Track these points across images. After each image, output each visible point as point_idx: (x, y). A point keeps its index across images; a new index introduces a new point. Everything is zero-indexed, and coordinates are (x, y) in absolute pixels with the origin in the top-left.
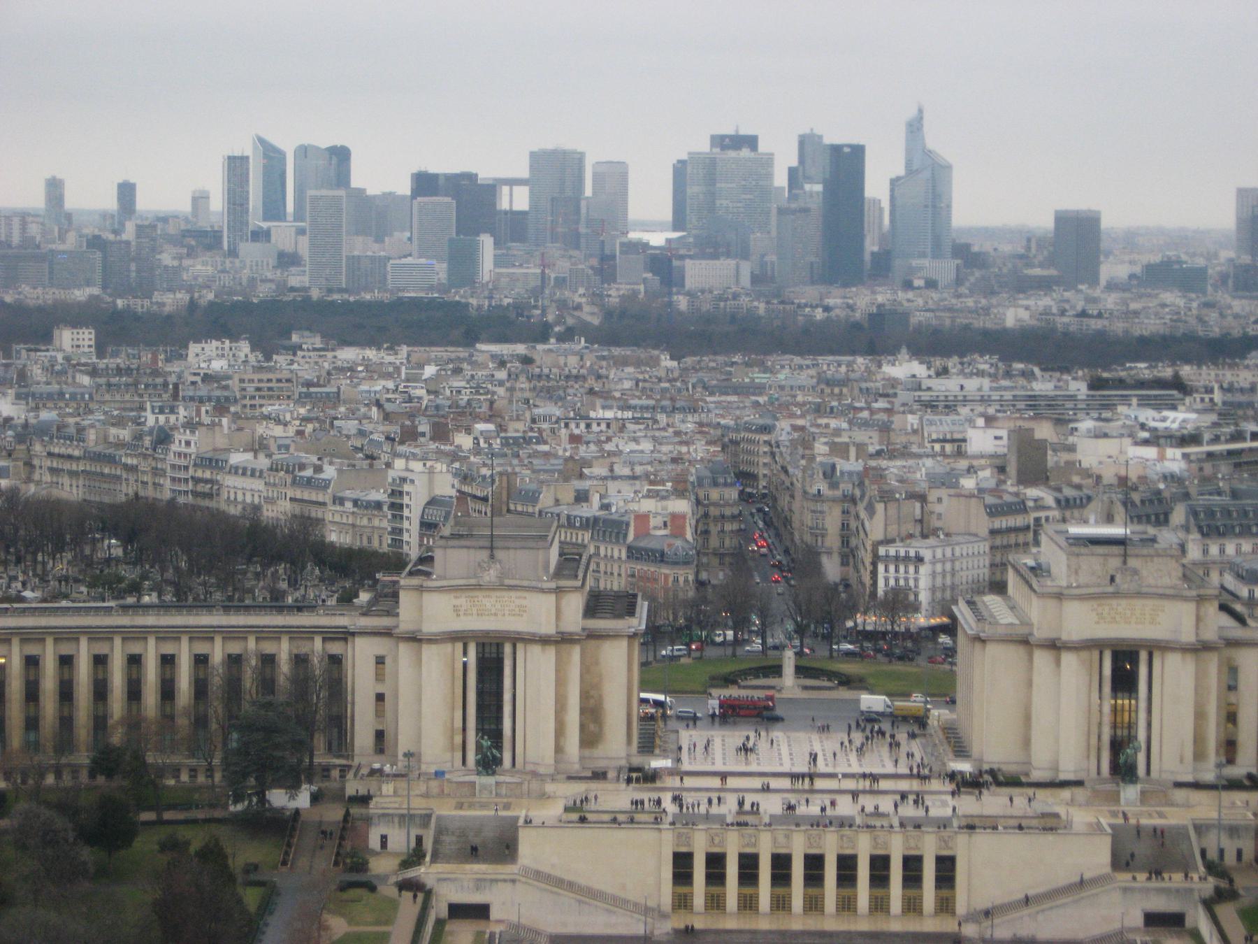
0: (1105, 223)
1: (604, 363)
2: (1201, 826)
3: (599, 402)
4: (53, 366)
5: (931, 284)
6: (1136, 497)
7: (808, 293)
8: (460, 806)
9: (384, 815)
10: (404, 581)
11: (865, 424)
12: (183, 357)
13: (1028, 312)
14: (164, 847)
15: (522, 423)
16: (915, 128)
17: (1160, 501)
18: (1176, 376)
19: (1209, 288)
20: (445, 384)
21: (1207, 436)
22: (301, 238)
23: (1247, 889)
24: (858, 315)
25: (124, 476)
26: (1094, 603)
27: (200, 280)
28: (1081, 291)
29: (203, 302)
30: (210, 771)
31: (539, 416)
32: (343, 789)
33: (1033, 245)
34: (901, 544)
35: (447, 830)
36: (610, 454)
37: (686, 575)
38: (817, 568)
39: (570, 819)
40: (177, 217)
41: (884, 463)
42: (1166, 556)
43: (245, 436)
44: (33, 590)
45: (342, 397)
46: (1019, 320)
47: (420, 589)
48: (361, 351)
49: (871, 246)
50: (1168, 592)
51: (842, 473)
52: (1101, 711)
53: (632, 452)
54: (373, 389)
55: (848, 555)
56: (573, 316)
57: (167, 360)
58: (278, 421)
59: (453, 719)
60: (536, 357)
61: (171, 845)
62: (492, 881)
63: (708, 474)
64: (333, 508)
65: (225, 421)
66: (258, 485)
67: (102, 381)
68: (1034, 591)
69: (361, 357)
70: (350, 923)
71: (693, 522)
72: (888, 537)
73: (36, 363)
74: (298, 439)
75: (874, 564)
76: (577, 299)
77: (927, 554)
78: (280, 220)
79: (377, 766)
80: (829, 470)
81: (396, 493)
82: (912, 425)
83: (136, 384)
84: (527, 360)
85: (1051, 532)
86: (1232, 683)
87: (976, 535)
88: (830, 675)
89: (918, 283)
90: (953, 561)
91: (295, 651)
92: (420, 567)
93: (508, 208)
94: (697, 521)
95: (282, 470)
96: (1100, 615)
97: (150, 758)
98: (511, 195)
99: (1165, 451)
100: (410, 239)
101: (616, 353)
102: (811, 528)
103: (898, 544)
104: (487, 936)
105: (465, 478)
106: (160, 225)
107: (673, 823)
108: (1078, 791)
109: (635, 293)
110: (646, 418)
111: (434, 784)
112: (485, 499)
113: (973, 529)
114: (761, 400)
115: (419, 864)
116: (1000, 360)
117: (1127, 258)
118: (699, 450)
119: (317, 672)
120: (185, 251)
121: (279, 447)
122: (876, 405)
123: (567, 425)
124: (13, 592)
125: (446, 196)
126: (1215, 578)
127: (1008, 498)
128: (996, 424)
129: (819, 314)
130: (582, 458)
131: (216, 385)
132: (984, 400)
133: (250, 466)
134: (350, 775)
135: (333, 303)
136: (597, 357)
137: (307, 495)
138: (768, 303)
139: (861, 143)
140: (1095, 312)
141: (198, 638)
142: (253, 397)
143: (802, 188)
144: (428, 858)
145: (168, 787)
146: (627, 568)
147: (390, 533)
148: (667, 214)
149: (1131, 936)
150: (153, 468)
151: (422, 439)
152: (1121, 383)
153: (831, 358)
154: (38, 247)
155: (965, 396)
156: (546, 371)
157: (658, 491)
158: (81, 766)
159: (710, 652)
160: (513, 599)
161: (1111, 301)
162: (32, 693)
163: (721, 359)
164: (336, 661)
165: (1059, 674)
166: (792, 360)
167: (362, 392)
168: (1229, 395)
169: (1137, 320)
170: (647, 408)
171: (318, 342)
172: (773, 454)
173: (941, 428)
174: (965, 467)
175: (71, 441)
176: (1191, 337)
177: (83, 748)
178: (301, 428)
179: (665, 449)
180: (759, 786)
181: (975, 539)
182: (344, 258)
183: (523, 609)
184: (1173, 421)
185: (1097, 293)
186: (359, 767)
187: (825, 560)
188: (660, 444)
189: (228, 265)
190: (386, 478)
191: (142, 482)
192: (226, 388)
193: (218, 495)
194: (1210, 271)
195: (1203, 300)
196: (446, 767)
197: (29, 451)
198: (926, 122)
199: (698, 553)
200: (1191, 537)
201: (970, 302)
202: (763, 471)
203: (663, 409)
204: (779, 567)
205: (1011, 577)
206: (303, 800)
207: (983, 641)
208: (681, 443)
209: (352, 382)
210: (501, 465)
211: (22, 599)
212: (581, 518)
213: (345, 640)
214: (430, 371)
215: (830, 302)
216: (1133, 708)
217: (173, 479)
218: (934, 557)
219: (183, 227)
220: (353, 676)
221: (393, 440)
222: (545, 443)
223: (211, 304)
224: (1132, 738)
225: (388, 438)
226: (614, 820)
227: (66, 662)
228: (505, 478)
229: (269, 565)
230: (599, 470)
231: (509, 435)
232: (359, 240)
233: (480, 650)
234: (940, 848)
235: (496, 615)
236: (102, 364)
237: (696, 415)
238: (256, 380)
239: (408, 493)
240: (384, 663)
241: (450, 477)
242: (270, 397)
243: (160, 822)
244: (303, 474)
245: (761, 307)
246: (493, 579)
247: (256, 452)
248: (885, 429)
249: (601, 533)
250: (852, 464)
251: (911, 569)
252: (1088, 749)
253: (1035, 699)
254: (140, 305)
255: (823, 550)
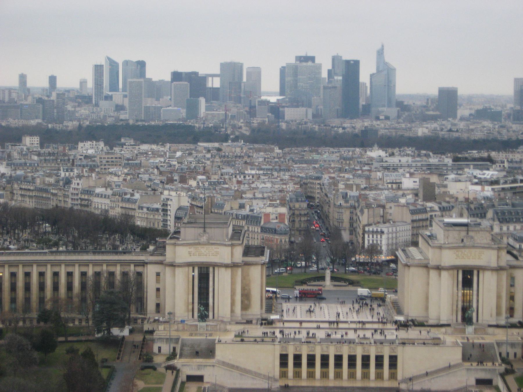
0: (459, 93)
1: (251, 151)
2: (499, 343)
3: (249, 167)
4: (22, 152)
5: (387, 118)
6: (472, 206)
7: (336, 122)
8: (191, 335)
9: (160, 338)
10: (168, 241)
11: (360, 176)
12: (76, 148)
13: (427, 130)
14: (68, 352)
15: (217, 176)
16: (380, 53)
17: (482, 208)
18: (489, 156)
19: (503, 120)
20: (185, 159)
21: (502, 181)
22: (125, 99)
23: (518, 369)
24: (357, 131)
25: (52, 198)
26: (455, 251)
27: (83, 116)
28: (449, 121)
29: (84, 126)
30: (87, 320)
31: (224, 173)
32: (143, 328)
33: (430, 102)
34: (375, 226)
35: (186, 344)
36: (254, 188)
37: (285, 239)
38: (340, 236)
39: (237, 340)
40: (73, 90)
41: (367, 192)
42: (485, 231)
43: (102, 181)
44: (14, 245)
45: (142, 165)
46: (424, 133)
47: (175, 245)
48: (150, 146)
49: (362, 102)
50: (486, 246)
51: (350, 196)
52: (458, 295)
53: (263, 188)
54: (155, 162)
55: (353, 231)
56: (238, 131)
57: (70, 150)
58: (116, 175)
59: (188, 299)
60: (223, 148)
61: (71, 351)
62: (205, 366)
63: (294, 197)
64: (138, 211)
65: (93, 175)
66: (107, 201)
67: (42, 158)
68: (430, 245)
69: (150, 148)
70: (145, 383)
71: (288, 217)
72: (369, 223)
73: (15, 151)
74: (124, 182)
75: (363, 234)
76: (240, 124)
77: (385, 230)
78: (116, 91)
79: (157, 318)
80: (345, 195)
81: (165, 205)
82: (379, 176)
83: (56, 160)
84: (219, 150)
85: (437, 221)
86: (512, 284)
87: (406, 222)
88: (345, 280)
89: (382, 117)
90: (396, 233)
91: (123, 270)
92: (174, 236)
93: (211, 86)
94: (290, 217)
95: (117, 195)
96: (457, 255)
97: (62, 315)
98: (212, 81)
99: (484, 187)
100: (170, 99)
101: (256, 147)
102: (337, 219)
103: (373, 226)
104: (202, 389)
105: (193, 199)
106: (66, 94)
107: (280, 342)
108: (448, 329)
109: (264, 122)
110: (269, 173)
111: (180, 326)
112: (202, 207)
113: (405, 220)
114: (317, 166)
115: (174, 359)
116: (416, 149)
117: (468, 107)
118: (291, 187)
119: (132, 279)
120: (77, 104)
121: (116, 186)
122: (364, 168)
123: (236, 177)
124: (5, 246)
125: (185, 81)
126: (505, 240)
127: (419, 207)
128: (414, 176)
129: (341, 131)
130: (242, 190)
131: (90, 160)
132: (409, 166)
133: (104, 194)
134: (146, 322)
135: (138, 126)
136: (248, 148)
137: (128, 205)
138: (319, 126)
139: (358, 59)
140: (455, 130)
141: (82, 265)
142: (105, 165)
143: (333, 78)
144: (178, 356)
145: (70, 327)
146: (261, 236)
147: (162, 221)
148: (277, 89)
149: (470, 389)
150: (63, 194)
151: (175, 182)
152: (466, 159)
153: (345, 149)
154: (16, 102)
155: (401, 165)
156: (227, 154)
157: (273, 204)
158: (34, 318)
159: (295, 271)
160: (213, 249)
161: (462, 125)
162: (13, 288)
163: (300, 149)
164: (140, 274)
165: (440, 280)
166: (329, 150)
167: (151, 163)
168: (511, 164)
169: (473, 133)
170: (269, 169)
171: (132, 142)
172: (321, 189)
173: (391, 178)
174: (401, 194)
175: (30, 183)
176: (495, 140)
177: (34, 310)
178: (125, 178)
179: (276, 186)
180: (316, 327)
181: (405, 224)
182: (143, 107)
183: (217, 253)
184: (488, 175)
185: (456, 122)
186: (149, 318)
187: (343, 232)
188: (275, 184)
189: (95, 110)
190: (160, 199)
191: (59, 200)
192: (94, 161)
193: (91, 205)
194: (503, 113)
195: (500, 124)
196: (186, 318)
197: (12, 187)
198: (385, 51)
199: (290, 230)
200: (495, 223)
201: (403, 126)
202: (317, 196)
203: (276, 170)
204: (324, 235)
205: (420, 240)
206: (126, 332)
207: (409, 266)
208: (283, 184)
209: (146, 158)
210: (208, 193)
211: (9, 249)
212: (241, 215)
213: (144, 266)
214: (179, 154)
215: (345, 125)
216: (471, 294)
217: (72, 199)
218: (388, 231)
219: (76, 94)
220: (147, 281)
221: (164, 183)
222: (227, 184)
223: (88, 126)
224: (470, 307)
225: (161, 182)
226: (255, 341)
227: (27, 275)
228: (210, 199)
229: (112, 235)
230: (249, 195)
231: (212, 180)
232: (149, 100)
233: (200, 270)
234: (391, 352)
235: (206, 255)
236: (42, 151)
237: (289, 172)
238: (106, 158)
239: (170, 205)
240: (159, 275)
241: (187, 198)
242: (112, 165)
243: (67, 341)
244: (126, 197)
245: (317, 128)
246: (205, 240)
247: (106, 188)
248: (368, 178)
249: (250, 221)
250: (354, 193)
251: (379, 236)
252: (453, 311)
253: (430, 290)
254: (58, 127)
255: (342, 228)
